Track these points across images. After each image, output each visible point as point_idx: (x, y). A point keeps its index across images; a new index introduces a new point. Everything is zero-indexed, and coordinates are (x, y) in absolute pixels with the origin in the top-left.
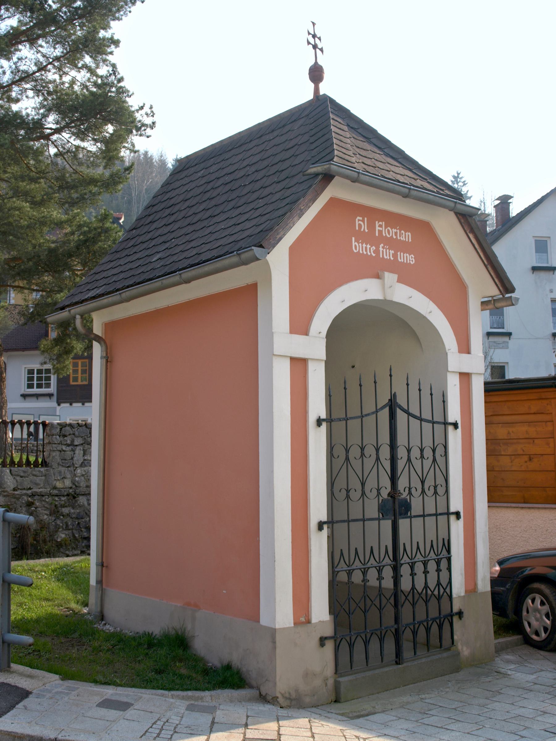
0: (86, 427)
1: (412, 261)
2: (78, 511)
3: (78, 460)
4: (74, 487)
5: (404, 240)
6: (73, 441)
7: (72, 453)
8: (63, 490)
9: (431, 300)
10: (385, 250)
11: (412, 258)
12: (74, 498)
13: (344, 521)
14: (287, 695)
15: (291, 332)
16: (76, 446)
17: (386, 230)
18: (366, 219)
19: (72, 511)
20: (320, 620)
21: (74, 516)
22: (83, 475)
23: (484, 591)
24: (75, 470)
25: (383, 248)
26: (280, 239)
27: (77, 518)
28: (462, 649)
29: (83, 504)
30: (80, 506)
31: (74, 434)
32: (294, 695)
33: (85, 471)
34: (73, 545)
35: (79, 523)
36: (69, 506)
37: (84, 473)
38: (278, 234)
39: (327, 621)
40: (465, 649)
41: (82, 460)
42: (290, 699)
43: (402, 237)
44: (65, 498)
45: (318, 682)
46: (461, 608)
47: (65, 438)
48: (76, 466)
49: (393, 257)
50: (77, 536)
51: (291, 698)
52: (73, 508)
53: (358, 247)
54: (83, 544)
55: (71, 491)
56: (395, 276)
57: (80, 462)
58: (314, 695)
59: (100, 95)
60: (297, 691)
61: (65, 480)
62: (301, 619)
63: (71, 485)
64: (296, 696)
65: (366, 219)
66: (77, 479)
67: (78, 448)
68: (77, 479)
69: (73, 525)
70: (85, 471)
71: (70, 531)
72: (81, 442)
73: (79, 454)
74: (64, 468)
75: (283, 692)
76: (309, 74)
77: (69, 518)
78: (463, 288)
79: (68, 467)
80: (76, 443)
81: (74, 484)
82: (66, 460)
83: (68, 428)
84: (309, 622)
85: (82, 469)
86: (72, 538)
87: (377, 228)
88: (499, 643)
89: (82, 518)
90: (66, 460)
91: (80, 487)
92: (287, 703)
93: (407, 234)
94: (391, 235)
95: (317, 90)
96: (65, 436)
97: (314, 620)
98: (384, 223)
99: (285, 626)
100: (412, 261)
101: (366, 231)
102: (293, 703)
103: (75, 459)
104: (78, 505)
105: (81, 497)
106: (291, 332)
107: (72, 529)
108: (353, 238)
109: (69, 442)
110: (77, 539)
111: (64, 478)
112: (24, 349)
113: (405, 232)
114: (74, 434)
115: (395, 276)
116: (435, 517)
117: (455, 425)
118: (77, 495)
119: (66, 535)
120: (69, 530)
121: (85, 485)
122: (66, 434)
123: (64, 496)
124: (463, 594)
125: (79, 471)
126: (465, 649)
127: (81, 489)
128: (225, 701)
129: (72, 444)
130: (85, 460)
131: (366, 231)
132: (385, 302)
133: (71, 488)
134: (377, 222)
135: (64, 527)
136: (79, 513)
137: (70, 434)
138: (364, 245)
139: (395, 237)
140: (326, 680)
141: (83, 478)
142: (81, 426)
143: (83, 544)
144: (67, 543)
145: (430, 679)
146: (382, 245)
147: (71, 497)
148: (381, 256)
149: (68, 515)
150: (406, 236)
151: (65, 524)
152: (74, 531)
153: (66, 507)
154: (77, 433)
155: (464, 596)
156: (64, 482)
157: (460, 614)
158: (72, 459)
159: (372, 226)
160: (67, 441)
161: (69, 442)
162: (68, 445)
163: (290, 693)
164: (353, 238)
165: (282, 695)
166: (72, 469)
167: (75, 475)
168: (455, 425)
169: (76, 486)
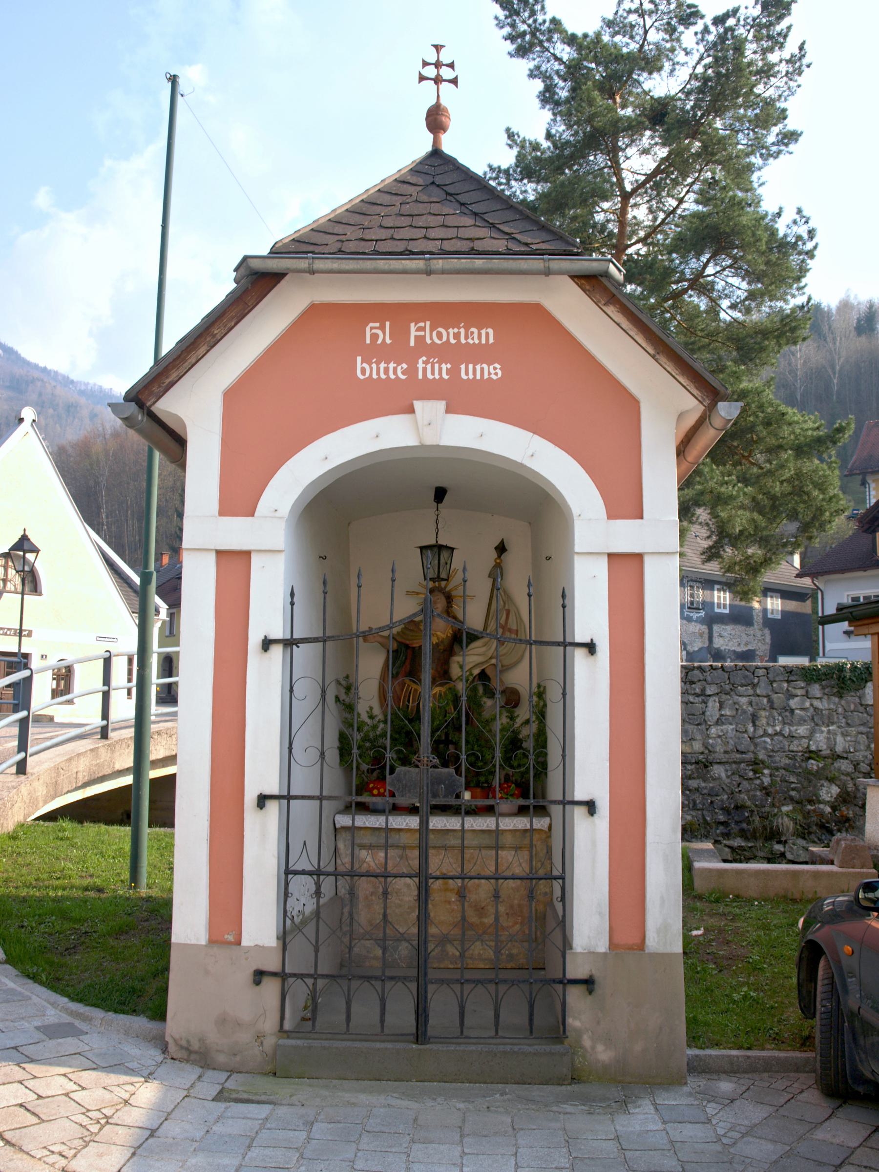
0: (723, 670)
1: (496, 374)
2: (711, 785)
3: (711, 716)
4: (707, 752)
5: (477, 341)
6: (703, 690)
7: (703, 705)
8: (689, 756)
9: (534, 433)
10: (429, 367)
11: (495, 369)
12: (706, 767)
13: (296, 797)
14: (184, 1043)
15: (222, 513)
16: (709, 696)
17: (434, 333)
18: (388, 324)
19: (703, 785)
20: (256, 943)
21: (705, 791)
22: (719, 737)
23: (662, 950)
24: (707, 729)
25: (426, 362)
26: (172, 384)
27: (709, 795)
28: (593, 1048)
29: (720, 775)
30: (714, 779)
31: (705, 680)
32: (196, 1046)
33: (722, 731)
34: (702, 831)
35: (712, 802)
36: (698, 778)
37: (721, 734)
38: (167, 378)
39: (271, 947)
40: (600, 1048)
41: (718, 716)
42: (187, 1049)
43: (473, 339)
44: (693, 766)
45: (244, 1037)
46: (594, 972)
47: (693, 686)
48: (709, 723)
49: (447, 374)
50: (708, 819)
51: (191, 1048)
52: (704, 781)
53: (363, 369)
54: (718, 831)
55: (701, 757)
56: (441, 405)
57: (715, 718)
58: (235, 1055)
59: (710, 214)
60: (202, 1040)
61: (694, 743)
62: (226, 936)
63: (702, 749)
64: (200, 1048)
65: (388, 324)
66: (710, 741)
67: (712, 699)
68: (710, 741)
69: (704, 804)
70: (722, 731)
71: (700, 812)
72: (716, 691)
73: (713, 707)
74: (692, 727)
75: (177, 1037)
76: (427, 119)
77: (697, 795)
78: (631, 405)
79: (698, 725)
80: (708, 692)
81: (706, 748)
82: (693, 715)
83: (696, 672)
84: (238, 943)
85: (719, 727)
86: (701, 821)
87: (413, 333)
88: (748, 1057)
89: (717, 795)
90: (693, 715)
91: (715, 752)
92: (183, 1054)
93: (483, 332)
94: (445, 339)
95: (436, 142)
96: (692, 683)
97: (245, 942)
98: (428, 323)
99: (189, 942)
100: (496, 374)
101: (388, 341)
102: (193, 1057)
103: (708, 713)
104: (711, 777)
105: (716, 767)
106: (222, 513)
107: (702, 809)
108: (359, 359)
109: (698, 691)
110: (708, 824)
111: (692, 739)
112: (843, 571)
113: (479, 330)
114: (705, 680)
115: (441, 405)
116: (291, 794)
117: (591, 648)
118: (711, 763)
119: (693, 816)
120: (698, 810)
121: (722, 750)
122: (693, 679)
123: (691, 764)
124: (602, 947)
125: (713, 731)
126: (600, 1048)
127: (716, 755)
128: (118, 1031)
129: (703, 693)
130: (722, 715)
131: (388, 341)
132: (422, 447)
133: (702, 753)
134: (412, 325)
135: (691, 806)
136: (713, 787)
137: (699, 681)
138: (382, 366)
139: (453, 341)
140: (259, 1037)
141: (719, 740)
142: (715, 669)
143: (718, 831)
144: (694, 827)
145: (485, 1083)
146: (424, 358)
147: (702, 766)
148: (420, 377)
149: (697, 790)
150: (488, 335)
151: (692, 802)
152: (705, 813)
153: (694, 778)
154: (709, 679)
155: (605, 954)
156: (692, 745)
157: (588, 983)
158: (703, 713)
159: (400, 333)
160: (695, 689)
161: (698, 691)
162: (698, 695)
163: (188, 1042)
164: (359, 359)
165: (175, 1041)
166: (703, 727)
167: (708, 736)
168: (591, 648)
169: (710, 751)
